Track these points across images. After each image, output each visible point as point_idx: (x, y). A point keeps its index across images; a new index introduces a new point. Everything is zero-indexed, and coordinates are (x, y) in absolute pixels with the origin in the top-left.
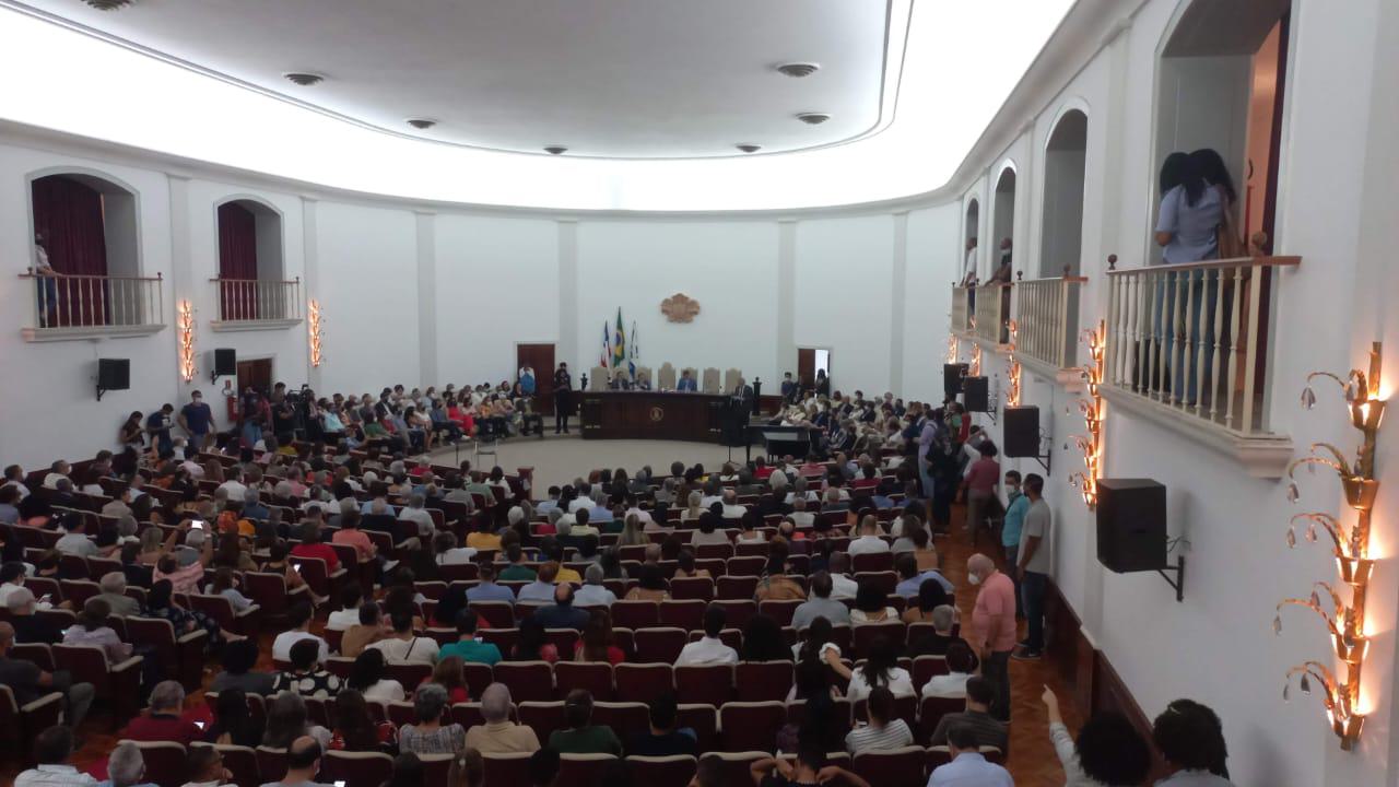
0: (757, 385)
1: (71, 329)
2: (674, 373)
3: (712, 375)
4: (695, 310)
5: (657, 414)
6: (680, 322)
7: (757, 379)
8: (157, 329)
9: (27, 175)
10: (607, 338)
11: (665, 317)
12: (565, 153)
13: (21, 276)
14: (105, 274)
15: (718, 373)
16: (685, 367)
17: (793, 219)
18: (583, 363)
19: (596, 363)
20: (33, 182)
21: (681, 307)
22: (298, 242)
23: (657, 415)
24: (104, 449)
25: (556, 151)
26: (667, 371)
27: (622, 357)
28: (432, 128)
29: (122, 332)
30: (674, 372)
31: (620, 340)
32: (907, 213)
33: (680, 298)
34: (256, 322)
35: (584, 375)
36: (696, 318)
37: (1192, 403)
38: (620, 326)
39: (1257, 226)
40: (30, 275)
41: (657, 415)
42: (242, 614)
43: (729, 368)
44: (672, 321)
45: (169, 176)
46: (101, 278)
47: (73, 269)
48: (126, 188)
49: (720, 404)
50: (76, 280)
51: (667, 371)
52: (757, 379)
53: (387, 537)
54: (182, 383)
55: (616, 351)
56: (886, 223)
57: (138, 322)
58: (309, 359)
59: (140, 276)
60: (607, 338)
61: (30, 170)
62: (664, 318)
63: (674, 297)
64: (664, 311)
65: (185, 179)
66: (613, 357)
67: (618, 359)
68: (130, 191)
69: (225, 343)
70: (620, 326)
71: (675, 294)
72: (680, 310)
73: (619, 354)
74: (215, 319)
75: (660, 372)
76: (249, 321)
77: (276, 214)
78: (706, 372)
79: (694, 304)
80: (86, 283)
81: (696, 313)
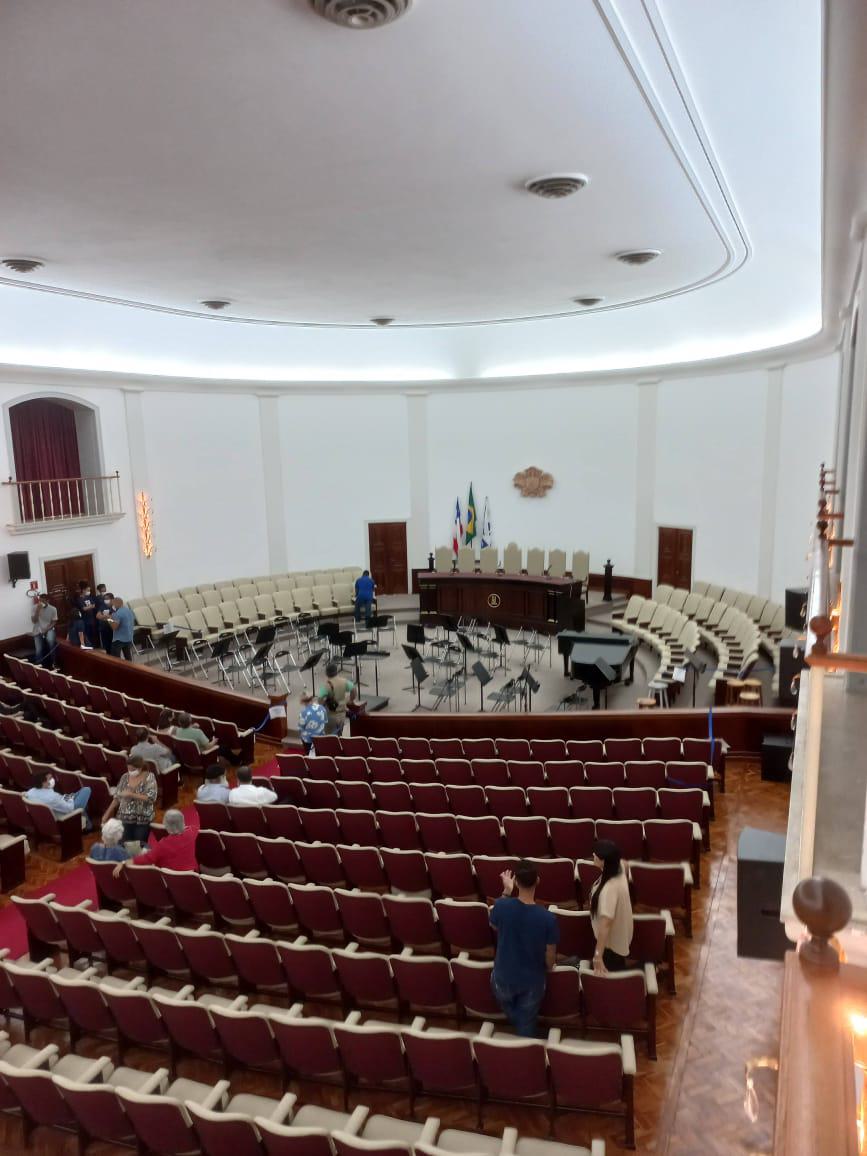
0: (609, 568)
1: (53, 520)
2: (519, 553)
3: (536, 555)
4: (549, 484)
5: (494, 601)
7: (609, 561)
9: (4, 405)
10: (459, 515)
11: (517, 492)
13: (4, 483)
14: (79, 476)
15: (543, 554)
17: (655, 379)
20: (11, 409)
21: (535, 480)
22: (113, 447)
23: (494, 601)
24: (559, 548)
26: (513, 552)
27: (475, 534)
29: (33, 529)
30: (520, 553)
31: (472, 516)
32: (783, 367)
33: (533, 472)
35: (431, 554)
36: (550, 493)
37: (664, 705)
40: (10, 483)
41: (494, 601)
43: (577, 550)
44: (524, 496)
45: (124, 391)
46: (77, 480)
48: (85, 404)
50: (56, 483)
51: (513, 552)
52: (609, 561)
55: (467, 528)
56: (760, 377)
57: (102, 511)
58: (140, 551)
59: (103, 475)
60: (459, 515)
61: (5, 401)
63: (527, 471)
64: (516, 485)
66: (465, 535)
67: (469, 538)
68: (91, 407)
71: (528, 467)
72: (534, 484)
73: (471, 531)
74: (11, 521)
75: (506, 552)
78: (551, 554)
79: (547, 477)
81: (550, 487)
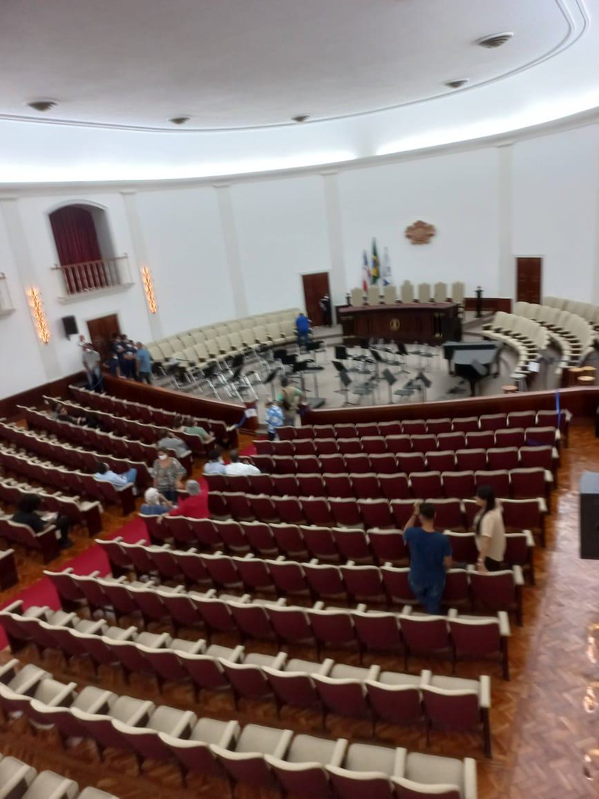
0: (479, 292)
6: (420, 244)
8: (130, 285)
10: (366, 263)
12: (307, 120)
16: (421, 282)
18: (345, 289)
19: (360, 286)
21: (420, 231)
23: (395, 325)
25: (300, 119)
26: (407, 287)
28: (187, 122)
31: (376, 264)
33: (420, 225)
34: (106, 289)
36: (433, 240)
38: (375, 253)
39: (350, 317)
41: (395, 325)
42: (207, 442)
44: (414, 244)
47: (71, 262)
49: (442, 314)
51: (407, 287)
53: (142, 465)
54: (42, 344)
58: (148, 309)
62: (408, 241)
64: (408, 237)
65: (13, 199)
67: (375, 279)
69: (66, 312)
70: (375, 253)
76: (100, 290)
77: (101, 210)
80: (73, 270)
81: (431, 235)
